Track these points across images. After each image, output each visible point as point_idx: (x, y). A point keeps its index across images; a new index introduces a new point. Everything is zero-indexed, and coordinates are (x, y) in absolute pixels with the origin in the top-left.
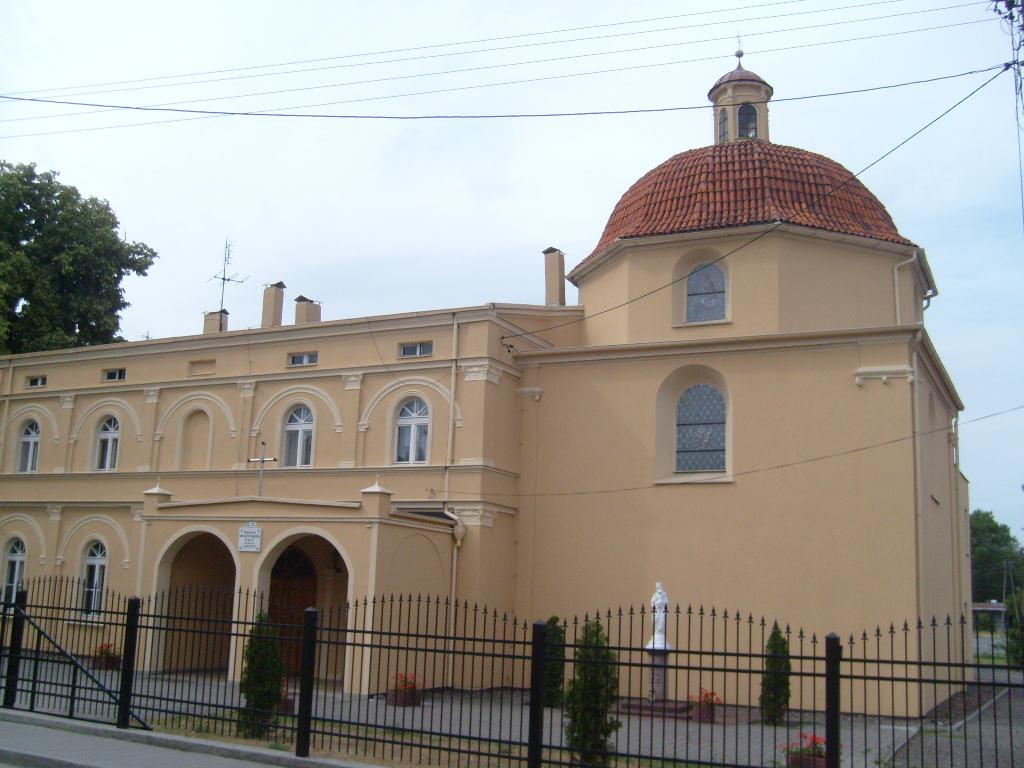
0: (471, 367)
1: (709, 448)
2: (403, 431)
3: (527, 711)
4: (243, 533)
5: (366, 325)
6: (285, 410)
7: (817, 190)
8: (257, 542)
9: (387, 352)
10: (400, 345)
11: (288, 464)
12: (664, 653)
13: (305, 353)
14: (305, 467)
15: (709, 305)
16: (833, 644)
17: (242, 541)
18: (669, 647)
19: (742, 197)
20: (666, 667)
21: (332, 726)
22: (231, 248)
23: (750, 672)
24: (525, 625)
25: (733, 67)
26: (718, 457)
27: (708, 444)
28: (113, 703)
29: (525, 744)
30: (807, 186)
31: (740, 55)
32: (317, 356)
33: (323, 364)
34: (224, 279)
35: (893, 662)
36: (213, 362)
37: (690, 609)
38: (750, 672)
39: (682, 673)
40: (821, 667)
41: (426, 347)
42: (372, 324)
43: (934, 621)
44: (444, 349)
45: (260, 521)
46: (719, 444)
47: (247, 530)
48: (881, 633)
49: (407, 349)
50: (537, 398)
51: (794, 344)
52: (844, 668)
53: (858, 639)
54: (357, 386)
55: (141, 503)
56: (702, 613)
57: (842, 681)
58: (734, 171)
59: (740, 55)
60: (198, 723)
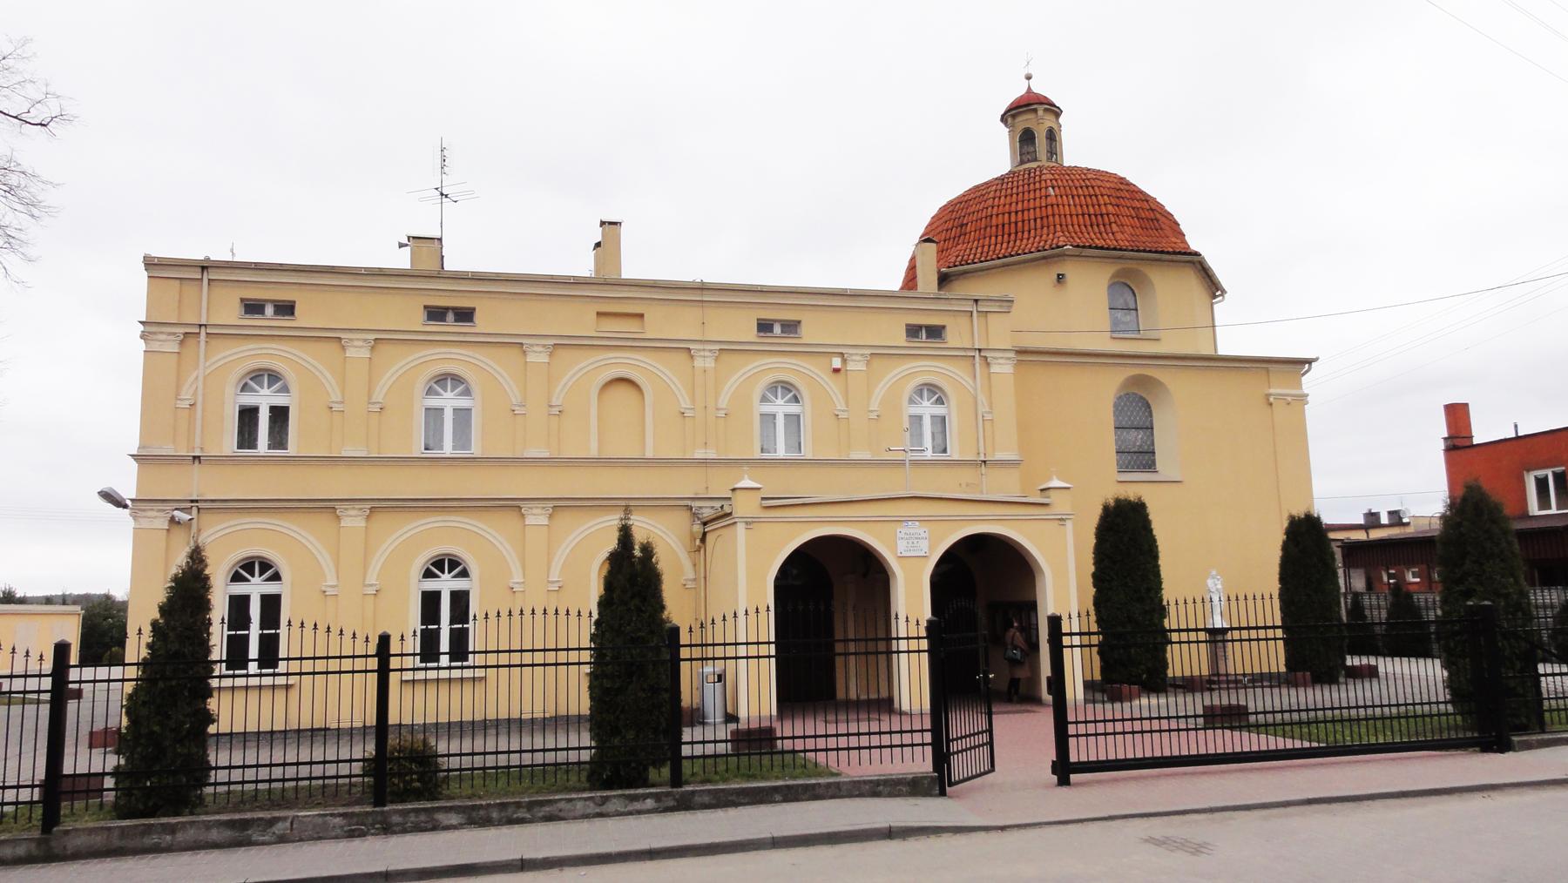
0: (155, 333)
1: (1141, 450)
2: (435, 414)
3: (393, 719)
4: (902, 535)
5: (699, 292)
9: (228, 312)
10: (907, 325)
12: (1223, 631)
13: (776, 321)
14: (942, 456)
16: (384, 640)
17: (902, 546)
18: (1225, 626)
19: (1066, 222)
20: (1225, 641)
21: (1558, 706)
24: (415, 632)
25: (1022, 91)
27: (1140, 446)
30: (1088, 198)
31: (1029, 78)
34: (442, 194)
35: (736, 644)
39: (1237, 644)
41: (791, 327)
42: (705, 292)
43: (510, 612)
44: (814, 330)
45: (924, 520)
48: (749, 613)
49: (436, 314)
50: (1271, 399)
51: (1206, 364)
52: (373, 663)
55: (730, 498)
57: (774, 654)
58: (1029, 192)
59: (1029, 78)
60: (721, 767)
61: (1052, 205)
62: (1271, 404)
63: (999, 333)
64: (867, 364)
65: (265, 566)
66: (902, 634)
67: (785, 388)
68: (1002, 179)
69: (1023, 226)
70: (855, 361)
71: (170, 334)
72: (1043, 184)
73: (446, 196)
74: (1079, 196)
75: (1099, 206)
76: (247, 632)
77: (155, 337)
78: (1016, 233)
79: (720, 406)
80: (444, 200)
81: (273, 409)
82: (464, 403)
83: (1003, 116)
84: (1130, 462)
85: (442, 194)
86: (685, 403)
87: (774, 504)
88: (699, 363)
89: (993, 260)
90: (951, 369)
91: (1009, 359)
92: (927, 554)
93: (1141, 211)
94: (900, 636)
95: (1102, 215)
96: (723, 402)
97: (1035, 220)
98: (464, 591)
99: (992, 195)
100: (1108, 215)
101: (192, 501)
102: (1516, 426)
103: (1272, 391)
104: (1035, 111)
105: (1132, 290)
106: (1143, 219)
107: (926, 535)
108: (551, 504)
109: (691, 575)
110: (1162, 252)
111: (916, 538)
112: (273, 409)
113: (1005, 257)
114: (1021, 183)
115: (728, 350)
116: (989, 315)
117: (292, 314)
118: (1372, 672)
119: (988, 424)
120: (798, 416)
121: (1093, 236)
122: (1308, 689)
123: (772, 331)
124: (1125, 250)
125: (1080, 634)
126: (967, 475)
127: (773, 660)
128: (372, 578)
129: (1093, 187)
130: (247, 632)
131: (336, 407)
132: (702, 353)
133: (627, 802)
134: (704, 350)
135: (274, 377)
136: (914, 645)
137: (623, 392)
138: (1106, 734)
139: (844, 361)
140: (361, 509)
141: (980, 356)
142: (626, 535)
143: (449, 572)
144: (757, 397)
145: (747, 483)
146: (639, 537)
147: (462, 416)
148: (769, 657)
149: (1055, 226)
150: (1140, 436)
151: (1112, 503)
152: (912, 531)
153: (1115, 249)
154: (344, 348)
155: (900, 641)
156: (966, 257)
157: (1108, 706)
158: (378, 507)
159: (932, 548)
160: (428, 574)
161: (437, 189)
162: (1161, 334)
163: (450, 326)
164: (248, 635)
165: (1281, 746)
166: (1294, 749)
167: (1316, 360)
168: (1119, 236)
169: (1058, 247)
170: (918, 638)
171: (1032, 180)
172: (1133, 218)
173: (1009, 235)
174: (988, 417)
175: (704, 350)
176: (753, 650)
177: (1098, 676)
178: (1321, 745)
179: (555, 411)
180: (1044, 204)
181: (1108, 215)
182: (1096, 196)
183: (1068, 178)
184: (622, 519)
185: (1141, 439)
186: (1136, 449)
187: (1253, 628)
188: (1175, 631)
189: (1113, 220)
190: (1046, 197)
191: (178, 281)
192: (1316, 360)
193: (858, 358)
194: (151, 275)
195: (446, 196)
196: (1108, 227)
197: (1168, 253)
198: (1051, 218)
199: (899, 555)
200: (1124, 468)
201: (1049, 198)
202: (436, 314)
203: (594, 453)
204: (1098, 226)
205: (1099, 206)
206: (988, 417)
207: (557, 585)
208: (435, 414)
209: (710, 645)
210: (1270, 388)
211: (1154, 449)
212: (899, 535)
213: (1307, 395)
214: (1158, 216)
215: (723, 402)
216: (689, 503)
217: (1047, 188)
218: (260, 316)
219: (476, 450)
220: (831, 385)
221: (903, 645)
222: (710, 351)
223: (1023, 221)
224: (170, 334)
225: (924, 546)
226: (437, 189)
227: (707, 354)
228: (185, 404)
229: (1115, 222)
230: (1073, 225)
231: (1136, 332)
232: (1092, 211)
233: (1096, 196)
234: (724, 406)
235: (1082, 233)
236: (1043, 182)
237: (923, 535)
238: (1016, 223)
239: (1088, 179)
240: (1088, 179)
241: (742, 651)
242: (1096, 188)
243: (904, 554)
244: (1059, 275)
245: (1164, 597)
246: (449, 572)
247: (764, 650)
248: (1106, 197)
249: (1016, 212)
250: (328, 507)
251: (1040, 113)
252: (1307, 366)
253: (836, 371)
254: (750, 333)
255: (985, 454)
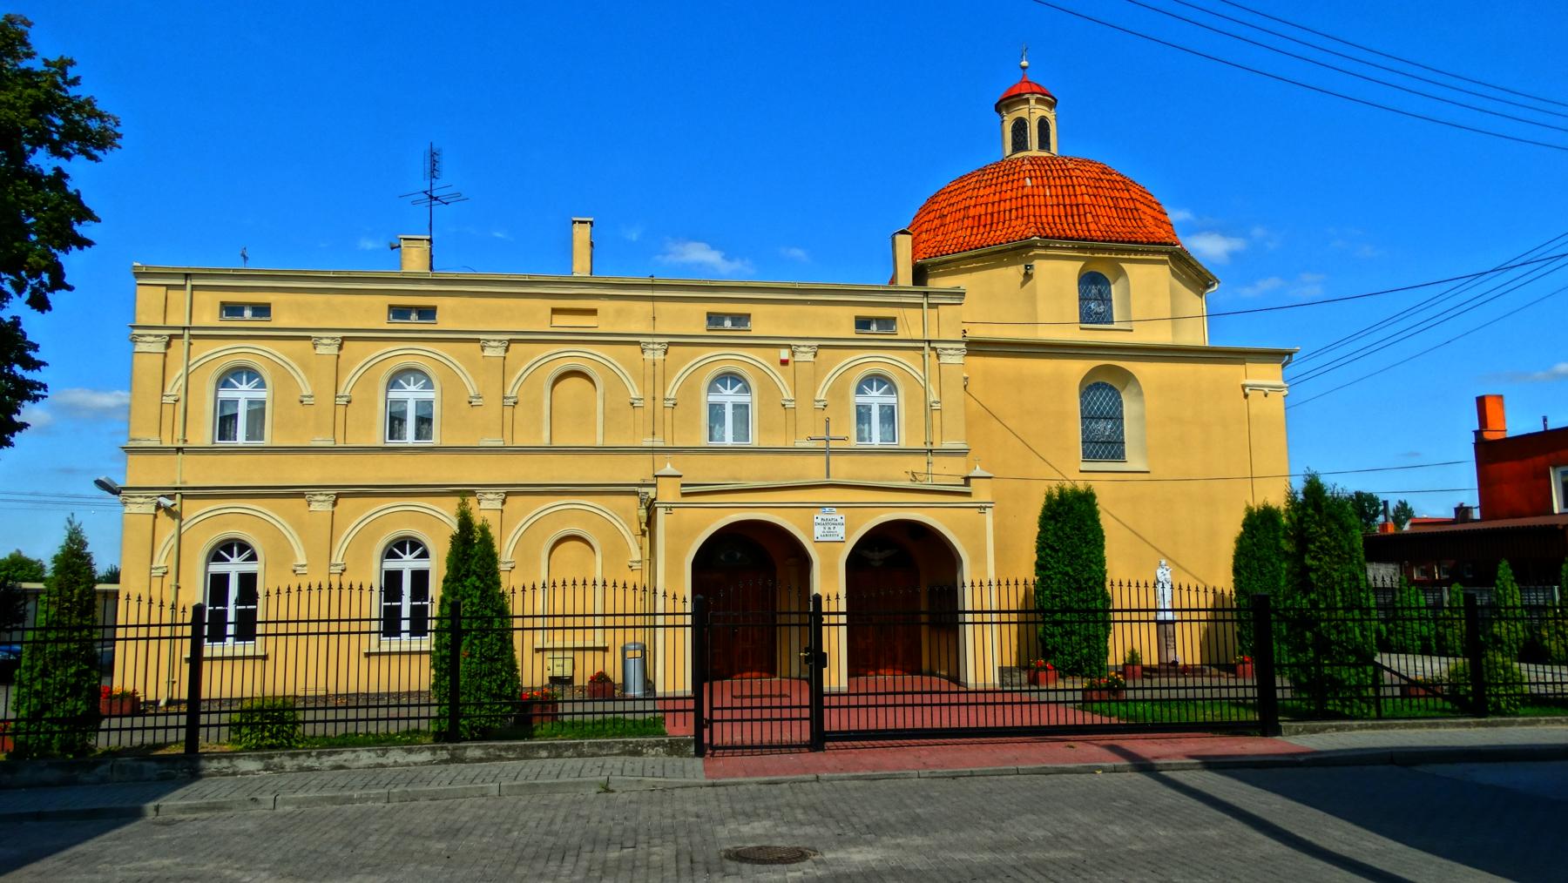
3: (204, 695)
4: (819, 521)
6: (714, 375)
7: (1078, 210)
8: (841, 531)
10: (856, 317)
11: (391, 437)
15: (1099, 311)
17: (818, 531)
22: (436, 158)
23: (1009, 623)
26: (1118, 448)
27: (1109, 436)
28: (1430, 696)
29: (827, 707)
32: (270, 308)
33: (443, 322)
34: (431, 197)
36: (593, 312)
37: (585, 581)
38: (1009, 623)
40: (188, 631)
46: (1118, 437)
47: (825, 517)
49: (399, 312)
50: (1247, 390)
53: (833, 597)
54: (334, 350)
56: (1129, 586)
57: (824, 628)
61: (1027, 196)
63: (947, 323)
65: (244, 547)
66: (518, 612)
67: (729, 378)
69: (999, 218)
70: (802, 352)
71: (156, 336)
72: (1022, 175)
73: (436, 199)
74: (1055, 186)
75: (1076, 196)
76: (254, 607)
77: (144, 339)
78: (992, 224)
79: (667, 396)
80: (434, 202)
81: (736, 406)
82: (743, 399)
83: (997, 106)
84: (1092, 452)
85: (431, 197)
86: (635, 393)
87: (692, 491)
89: (965, 251)
90: (438, 351)
91: (959, 349)
93: (1120, 200)
94: (658, 612)
95: (1077, 205)
96: (671, 392)
97: (1010, 211)
99: (972, 186)
100: (1083, 205)
101: (176, 488)
102: (1545, 420)
103: (1248, 382)
104: (1027, 101)
106: (1121, 209)
107: (843, 521)
108: (335, 491)
109: (638, 558)
110: (1136, 242)
112: (736, 406)
113: (976, 248)
114: (1001, 173)
115: (346, 338)
116: (940, 307)
117: (269, 315)
120: (747, 406)
121: (1065, 226)
122: (271, 694)
123: (242, 315)
124: (1096, 241)
125: (1173, 610)
126: (917, 464)
127: (689, 630)
128: (337, 558)
129: (1071, 178)
130: (254, 607)
131: (789, 405)
132: (651, 346)
133: (405, 754)
134: (654, 343)
135: (251, 373)
136: (833, 619)
138: (968, 704)
139: (793, 354)
140: (327, 495)
142: (465, 522)
143: (411, 554)
144: (705, 384)
145: (669, 469)
146: (477, 521)
147: (741, 410)
148: (685, 626)
149: (1028, 217)
151: (1056, 493)
152: (829, 517)
153: (1085, 240)
154: (938, 356)
155: (658, 617)
156: (941, 249)
157: (908, 678)
158: (343, 492)
159: (849, 532)
160: (390, 554)
161: (425, 192)
162: (1135, 326)
163: (414, 323)
164: (400, 606)
165: (1079, 722)
166: (1101, 725)
168: (1093, 226)
169: (1026, 238)
170: (685, 614)
171: (1012, 171)
172: (1110, 208)
173: (985, 226)
174: (936, 406)
175: (654, 343)
176: (589, 622)
178: (1121, 722)
180: (1020, 195)
181: (1083, 205)
182: (1074, 186)
183: (1047, 168)
184: (459, 505)
186: (1104, 439)
187: (1004, 612)
188: (969, 612)
189: (1088, 210)
190: (1023, 187)
191: (165, 288)
193: (496, 344)
195: (436, 199)
196: (1082, 217)
197: (1142, 243)
198: (1025, 209)
200: (1088, 456)
201: (1026, 189)
202: (399, 312)
203: (544, 441)
204: (1072, 216)
205: (1076, 196)
207: (510, 565)
208: (716, 412)
209: (179, 625)
214: (1138, 205)
215: (671, 392)
216: (636, 489)
217: (1024, 178)
218: (239, 318)
219: (754, 440)
220: (781, 379)
221: (969, 618)
222: (660, 344)
223: (999, 212)
224: (156, 336)
225: (841, 531)
226: (425, 192)
227: (656, 346)
228: (170, 400)
229: (1091, 213)
230: (1072, 216)
231: (1105, 318)
232: (1067, 202)
233: (1074, 186)
234: (672, 396)
235: (1055, 224)
236: (1022, 173)
237: (840, 521)
238: (992, 214)
239: (1068, 170)
240: (1068, 170)
241: (599, 621)
242: (1074, 178)
245: (1107, 576)
246: (411, 554)
247: (679, 620)
248: (1083, 187)
249: (993, 204)
250: (296, 492)
251: (1032, 102)
252: (1287, 357)
253: (784, 362)
254: (848, 330)
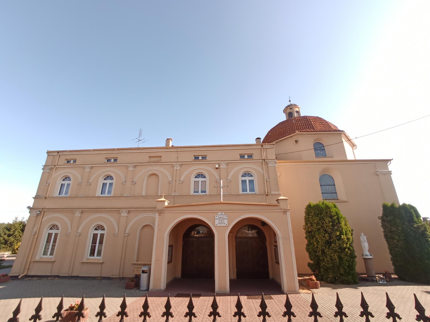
4: (217, 218)
13: (200, 156)
17: (217, 222)
62: (378, 175)
64: (227, 166)
68: (285, 121)
88: (175, 168)
92: (227, 225)
96: (182, 179)
98: (55, 234)
105: (321, 143)
111: (223, 219)
114: (290, 122)
118: (333, 276)
119: (268, 183)
137: (153, 177)
141: (264, 162)
150: (330, 188)
167: (392, 159)
177: (235, 277)
179: (134, 183)
185: (331, 189)
192: (392, 159)
194: (48, 155)
199: (216, 225)
206: (268, 180)
210: (376, 170)
211: (321, 188)
212: (216, 218)
213: (391, 171)
237: (225, 218)
238: (284, 131)
243: (217, 225)
244: (296, 141)
253: (217, 168)
255: (267, 192)
